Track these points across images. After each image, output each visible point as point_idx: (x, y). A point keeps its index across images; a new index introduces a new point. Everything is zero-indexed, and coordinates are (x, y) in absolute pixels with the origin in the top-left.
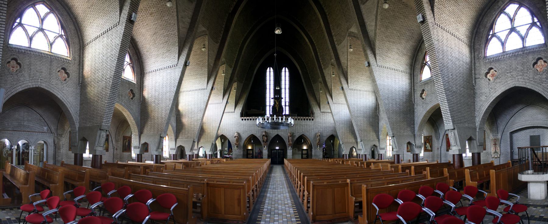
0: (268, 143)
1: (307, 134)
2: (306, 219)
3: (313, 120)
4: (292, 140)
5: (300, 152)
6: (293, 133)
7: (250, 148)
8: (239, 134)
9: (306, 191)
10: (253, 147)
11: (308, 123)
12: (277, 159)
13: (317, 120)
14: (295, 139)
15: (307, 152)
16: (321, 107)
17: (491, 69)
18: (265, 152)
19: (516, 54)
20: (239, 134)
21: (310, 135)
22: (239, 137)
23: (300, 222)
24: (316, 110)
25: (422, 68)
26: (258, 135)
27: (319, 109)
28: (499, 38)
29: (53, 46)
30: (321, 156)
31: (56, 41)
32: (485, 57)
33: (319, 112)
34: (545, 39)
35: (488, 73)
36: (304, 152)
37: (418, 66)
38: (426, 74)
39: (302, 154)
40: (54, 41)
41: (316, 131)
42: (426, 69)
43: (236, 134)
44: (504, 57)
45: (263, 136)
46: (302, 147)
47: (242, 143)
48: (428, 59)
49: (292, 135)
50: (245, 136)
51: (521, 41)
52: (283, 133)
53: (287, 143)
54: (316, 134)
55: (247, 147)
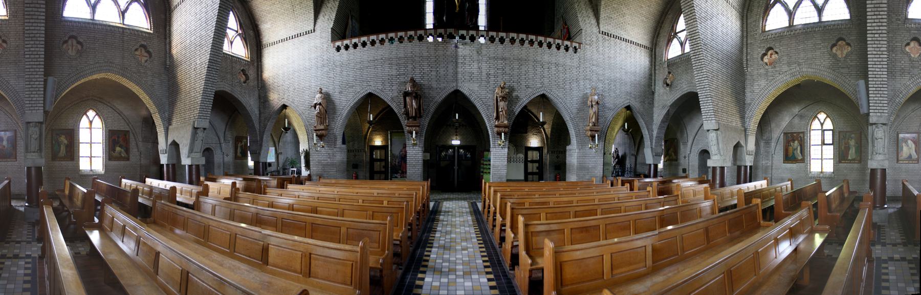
0: (426, 121)
1: (556, 96)
2: (509, 282)
3: (575, 50)
4: (509, 112)
5: (522, 156)
6: (512, 90)
7: (378, 141)
8: (327, 97)
9: (508, 230)
10: (386, 140)
11: (561, 60)
12: (457, 174)
13: (588, 53)
14: (517, 109)
15: (541, 156)
16: (603, 15)
17: (771, 48)
18: (415, 154)
19: (809, 29)
20: (327, 97)
21: (567, 104)
22: (327, 107)
23: (496, 292)
24: (586, 23)
25: (669, 41)
26: (390, 95)
27: (594, 21)
28: (785, 6)
29: (126, 15)
30: (599, 171)
31: (131, 7)
32: (764, 31)
33: (595, 30)
34: (850, 12)
35: (765, 54)
36: (535, 155)
37: (662, 41)
38: (674, 50)
39: (526, 162)
40: (127, 8)
41: (585, 87)
42: (675, 42)
43: (318, 98)
44: (792, 33)
45: (406, 94)
46: (525, 139)
47: (338, 126)
48: (681, 24)
49: (508, 96)
50: (345, 103)
51: (815, 13)
52: (475, 87)
53: (490, 125)
54: (585, 98)
55: (371, 140)
